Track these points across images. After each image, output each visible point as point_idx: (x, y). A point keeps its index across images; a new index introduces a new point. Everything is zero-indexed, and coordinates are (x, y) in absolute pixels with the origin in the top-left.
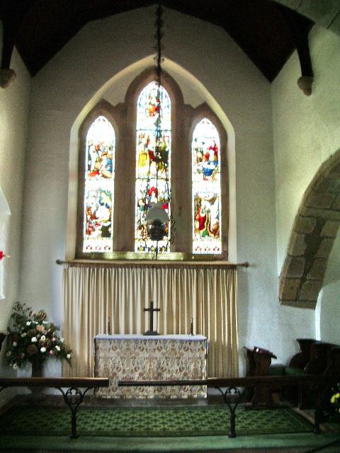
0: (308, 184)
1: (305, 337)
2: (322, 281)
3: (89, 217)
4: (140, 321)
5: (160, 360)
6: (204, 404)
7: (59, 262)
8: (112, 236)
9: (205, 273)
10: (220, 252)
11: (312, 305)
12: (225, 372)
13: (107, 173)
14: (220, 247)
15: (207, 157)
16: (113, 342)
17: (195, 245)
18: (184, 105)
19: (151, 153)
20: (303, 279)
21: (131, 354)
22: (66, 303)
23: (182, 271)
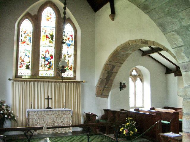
0: (111, 53)
2: (111, 88)
3: (21, 61)
4: (43, 103)
5: (54, 119)
6: (71, 134)
7: (10, 80)
8: (30, 69)
9: (69, 85)
10: (73, 76)
11: (107, 97)
12: (75, 123)
13: (29, 43)
14: (73, 75)
15: (69, 39)
16: (53, 112)
19: (47, 36)
20: (105, 87)
21: (42, 116)
22: (19, 96)
23: (60, 83)
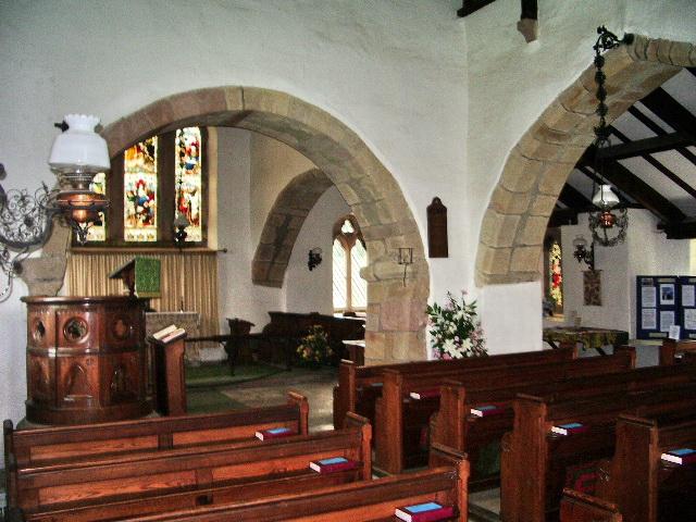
1: (274, 309)
17: (127, 233)
18: (576, 215)
